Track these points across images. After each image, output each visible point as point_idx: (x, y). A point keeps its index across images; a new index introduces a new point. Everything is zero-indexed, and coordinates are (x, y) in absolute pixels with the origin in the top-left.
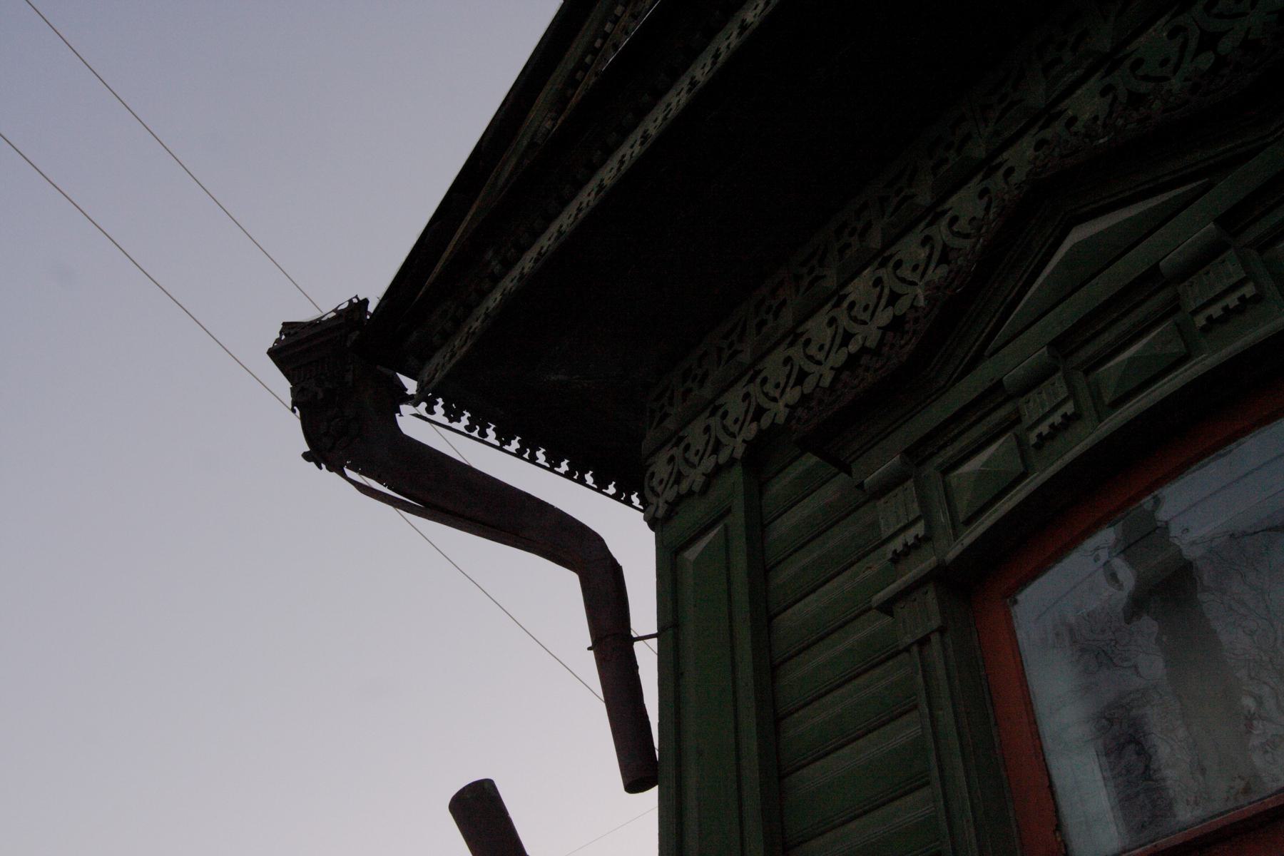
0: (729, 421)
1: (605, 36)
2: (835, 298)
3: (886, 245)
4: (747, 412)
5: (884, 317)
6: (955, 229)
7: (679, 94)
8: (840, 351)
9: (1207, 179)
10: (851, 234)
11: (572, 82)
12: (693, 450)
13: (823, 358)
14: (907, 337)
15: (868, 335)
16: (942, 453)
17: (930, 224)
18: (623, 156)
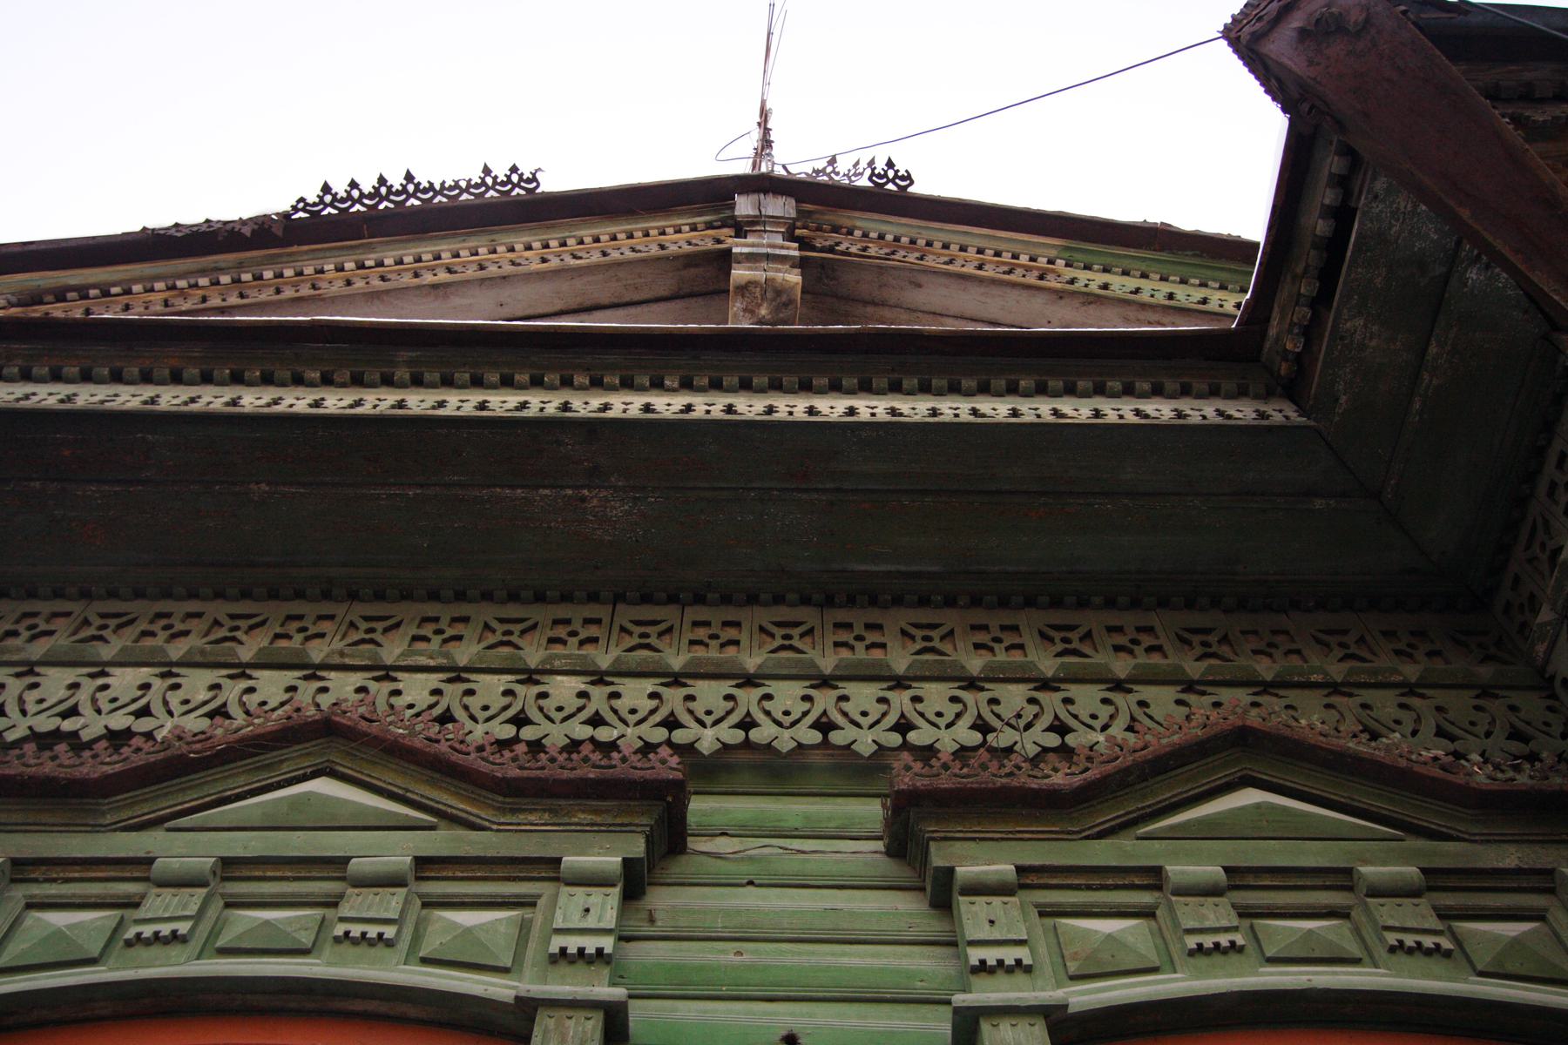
1: (128, 292)
3: (179, 664)
5: (119, 721)
6: (245, 698)
7: (133, 396)
8: (53, 719)
9: (435, 820)
10: (165, 628)
11: (60, 295)
12: (109, 694)
13: (32, 712)
14: (115, 758)
15: (90, 725)
16: (46, 885)
17: (231, 677)
18: (34, 394)
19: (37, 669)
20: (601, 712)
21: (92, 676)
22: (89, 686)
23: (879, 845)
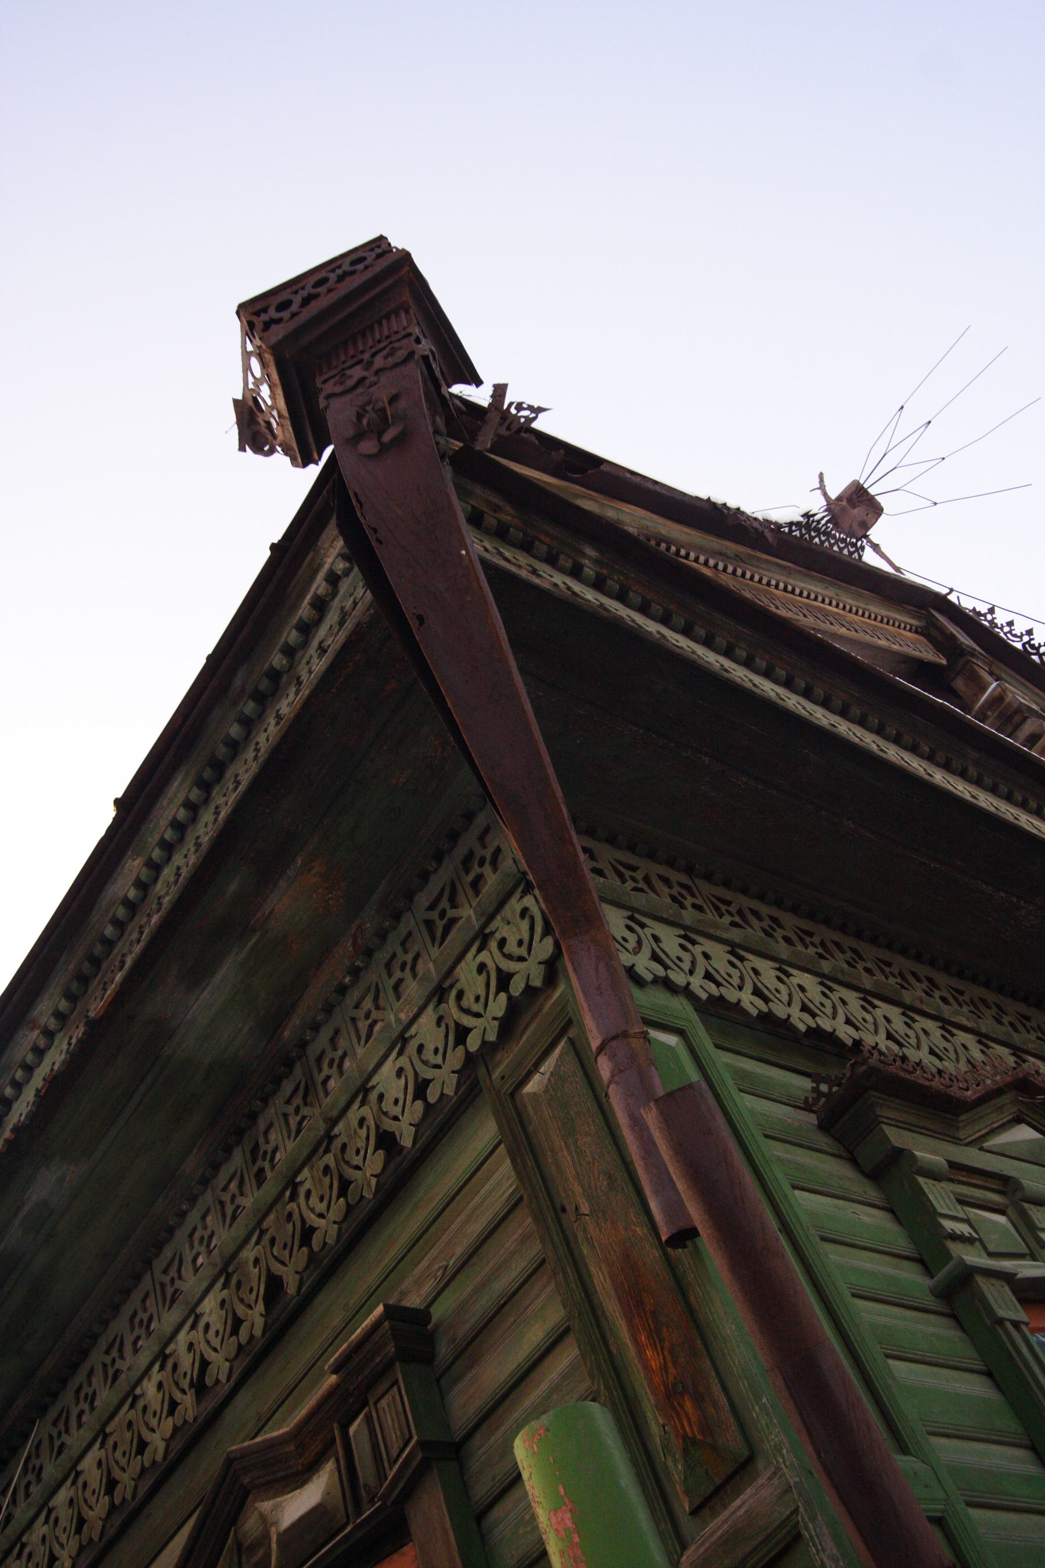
0: (468, 1001)
2: (19, 1545)
3: (486, 925)
4: (447, 1036)
12: (429, 1048)
19: (168, 1351)
20: (149, 1446)
21: (193, 1327)
22: (198, 1335)
23: (813, 1119)
